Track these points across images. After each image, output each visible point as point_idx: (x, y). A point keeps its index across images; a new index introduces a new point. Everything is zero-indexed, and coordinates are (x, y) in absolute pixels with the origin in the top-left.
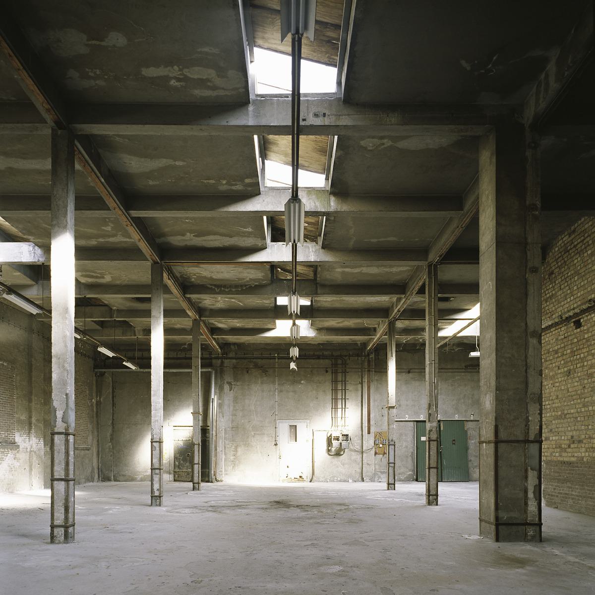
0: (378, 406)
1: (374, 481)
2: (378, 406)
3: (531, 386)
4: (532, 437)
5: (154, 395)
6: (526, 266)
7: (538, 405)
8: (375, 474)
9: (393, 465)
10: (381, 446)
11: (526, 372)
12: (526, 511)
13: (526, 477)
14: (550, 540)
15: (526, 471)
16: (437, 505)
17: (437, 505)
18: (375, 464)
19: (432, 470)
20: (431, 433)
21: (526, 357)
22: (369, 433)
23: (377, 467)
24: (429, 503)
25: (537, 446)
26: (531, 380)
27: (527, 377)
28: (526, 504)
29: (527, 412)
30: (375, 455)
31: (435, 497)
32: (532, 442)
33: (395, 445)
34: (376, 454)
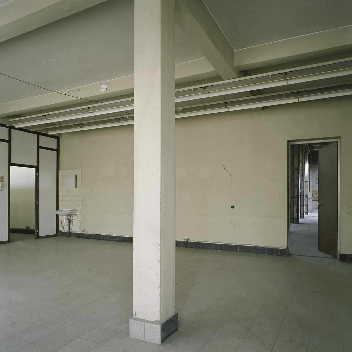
0: (314, 179)
1: (312, 213)
2: (314, 179)
3: (295, 183)
4: (295, 196)
5: (134, 248)
6: (294, 151)
7: (297, 188)
8: (313, 210)
9: (307, 205)
10: (316, 197)
11: (294, 179)
12: (293, 215)
13: (294, 207)
14: (299, 223)
15: (294, 205)
16: (304, 218)
17: (304, 218)
18: (313, 205)
19: (302, 206)
20: (302, 193)
21: (294, 175)
22: (310, 191)
23: (314, 206)
24: (75, 187)
25: (297, 198)
26: (295, 181)
27: (294, 180)
28: (294, 214)
29: (294, 189)
30: (313, 201)
31: (303, 216)
32: (295, 197)
33: (308, 197)
34: (313, 200)
